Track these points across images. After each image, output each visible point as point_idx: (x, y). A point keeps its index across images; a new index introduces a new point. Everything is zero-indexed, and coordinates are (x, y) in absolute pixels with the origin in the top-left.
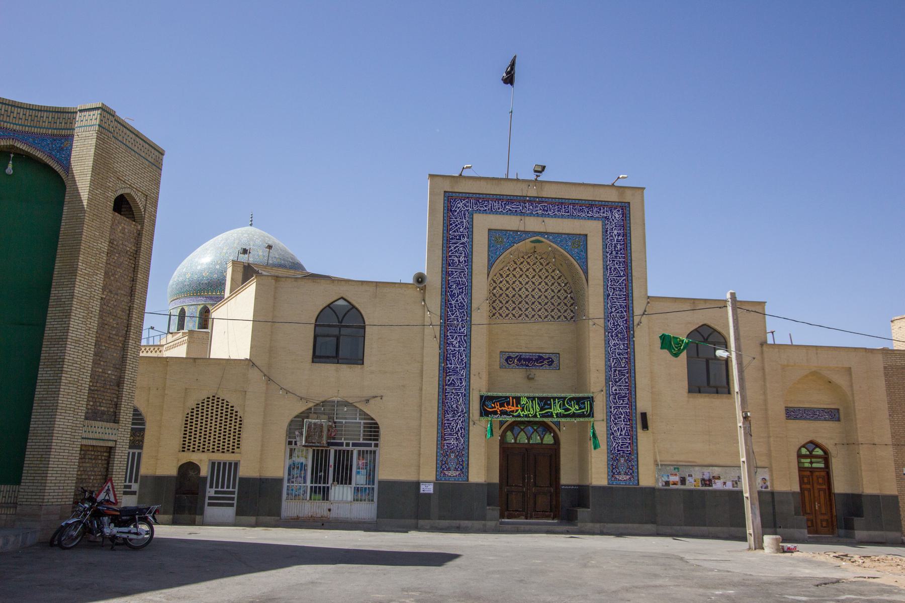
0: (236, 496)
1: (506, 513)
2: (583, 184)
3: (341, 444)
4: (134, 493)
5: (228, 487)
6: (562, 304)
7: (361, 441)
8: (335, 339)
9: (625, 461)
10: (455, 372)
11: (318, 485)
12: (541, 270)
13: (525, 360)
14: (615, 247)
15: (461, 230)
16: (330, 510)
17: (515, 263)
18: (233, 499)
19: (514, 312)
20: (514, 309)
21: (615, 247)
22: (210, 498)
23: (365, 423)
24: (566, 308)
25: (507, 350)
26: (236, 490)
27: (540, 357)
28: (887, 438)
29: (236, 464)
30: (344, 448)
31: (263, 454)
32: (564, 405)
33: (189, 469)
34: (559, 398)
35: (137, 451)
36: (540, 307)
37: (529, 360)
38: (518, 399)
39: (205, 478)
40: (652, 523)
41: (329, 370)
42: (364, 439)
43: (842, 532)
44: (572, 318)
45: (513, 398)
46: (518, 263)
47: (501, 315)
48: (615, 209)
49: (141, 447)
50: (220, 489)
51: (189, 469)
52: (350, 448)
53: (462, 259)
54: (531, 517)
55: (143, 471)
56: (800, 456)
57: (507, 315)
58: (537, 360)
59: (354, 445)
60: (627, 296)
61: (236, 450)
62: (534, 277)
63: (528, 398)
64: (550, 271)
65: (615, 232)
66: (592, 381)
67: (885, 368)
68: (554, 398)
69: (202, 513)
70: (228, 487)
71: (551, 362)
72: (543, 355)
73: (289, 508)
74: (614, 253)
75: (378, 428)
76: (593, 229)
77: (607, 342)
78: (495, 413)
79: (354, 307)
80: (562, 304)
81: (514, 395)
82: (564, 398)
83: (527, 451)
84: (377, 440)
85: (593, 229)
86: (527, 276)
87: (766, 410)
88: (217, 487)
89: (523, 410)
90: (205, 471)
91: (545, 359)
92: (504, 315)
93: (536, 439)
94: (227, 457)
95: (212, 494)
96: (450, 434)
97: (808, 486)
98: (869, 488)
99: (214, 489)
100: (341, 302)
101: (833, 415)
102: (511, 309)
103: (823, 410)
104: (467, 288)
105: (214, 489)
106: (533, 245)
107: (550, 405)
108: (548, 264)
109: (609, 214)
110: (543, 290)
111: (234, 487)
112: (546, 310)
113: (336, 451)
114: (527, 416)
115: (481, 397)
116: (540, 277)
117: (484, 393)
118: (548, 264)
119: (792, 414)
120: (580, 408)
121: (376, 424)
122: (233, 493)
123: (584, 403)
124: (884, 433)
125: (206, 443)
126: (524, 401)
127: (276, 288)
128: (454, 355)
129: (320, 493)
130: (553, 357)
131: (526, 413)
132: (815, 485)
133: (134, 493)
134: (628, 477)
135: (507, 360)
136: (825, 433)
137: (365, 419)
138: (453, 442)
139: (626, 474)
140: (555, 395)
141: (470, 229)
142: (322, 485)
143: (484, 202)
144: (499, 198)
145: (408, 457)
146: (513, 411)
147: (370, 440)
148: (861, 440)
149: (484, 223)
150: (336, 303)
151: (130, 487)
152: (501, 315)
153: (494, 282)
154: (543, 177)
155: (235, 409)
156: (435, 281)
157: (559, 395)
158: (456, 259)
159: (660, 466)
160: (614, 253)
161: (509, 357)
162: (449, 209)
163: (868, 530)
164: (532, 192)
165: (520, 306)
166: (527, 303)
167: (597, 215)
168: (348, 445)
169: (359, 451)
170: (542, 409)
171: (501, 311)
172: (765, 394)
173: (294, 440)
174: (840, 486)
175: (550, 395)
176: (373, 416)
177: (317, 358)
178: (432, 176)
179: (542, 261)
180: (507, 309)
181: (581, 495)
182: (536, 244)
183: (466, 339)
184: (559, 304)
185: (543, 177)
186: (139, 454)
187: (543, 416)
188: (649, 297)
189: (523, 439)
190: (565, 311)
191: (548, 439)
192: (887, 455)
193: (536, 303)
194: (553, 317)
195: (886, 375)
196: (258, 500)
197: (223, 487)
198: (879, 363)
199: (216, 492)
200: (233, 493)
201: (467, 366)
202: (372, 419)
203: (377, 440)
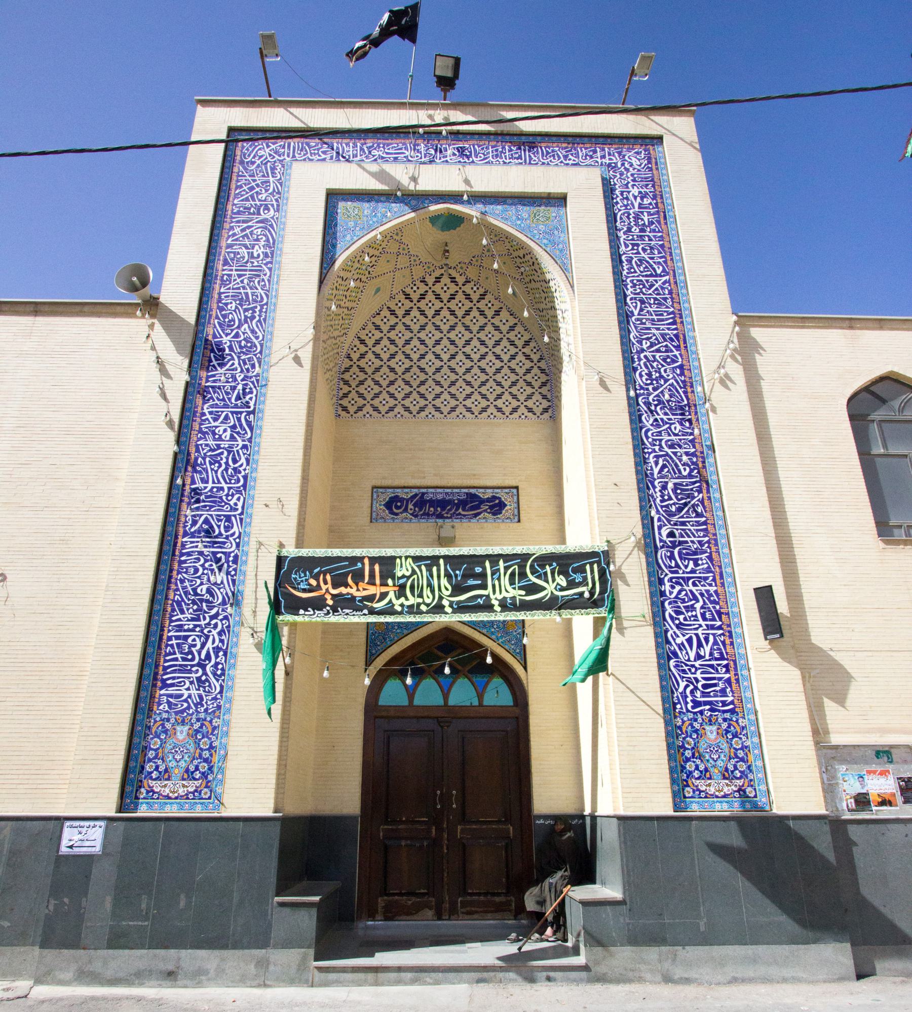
1: (381, 902)
13: (432, 503)
14: (637, 217)
15: (263, 196)
21: (637, 217)
25: (388, 483)
27: (473, 497)
32: (523, 575)
34: (507, 558)
38: (388, 564)
44: (546, 410)
45: (373, 560)
46: (415, 297)
54: (453, 913)
58: (463, 504)
62: (452, 328)
63: (416, 559)
64: (490, 313)
65: (635, 191)
68: (494, 559)
72: (401, 493)
74: (636, 230)
78: (318, 604)
81: (375, 552)
82: (525, 557)
89: (401, 593)
91: (482, 501)
96: (183, 669)
107: (483, 575)
109: (616, 159)
114: (413, 610)
115: (280, 560)
116: (467, 328)
117: (291, 551)
120: (571, 584)
123: (581, 570)
126: (403, 569)
128: (215, 461)
130: (503, 495)
131: (412, 600)
134: (192, 786)
135: (388, 505)
140: (497, 550)
146: (371, 598)
153: (362, 342)
157: (508, 550)
159: (831, 756)
160: (636, 230)
170: (458, 589)
175: (480, 551)
179: (467, 289)
183: (246, 416)
187: (461, 608)
189: (429, 694)
191: (497, 695)
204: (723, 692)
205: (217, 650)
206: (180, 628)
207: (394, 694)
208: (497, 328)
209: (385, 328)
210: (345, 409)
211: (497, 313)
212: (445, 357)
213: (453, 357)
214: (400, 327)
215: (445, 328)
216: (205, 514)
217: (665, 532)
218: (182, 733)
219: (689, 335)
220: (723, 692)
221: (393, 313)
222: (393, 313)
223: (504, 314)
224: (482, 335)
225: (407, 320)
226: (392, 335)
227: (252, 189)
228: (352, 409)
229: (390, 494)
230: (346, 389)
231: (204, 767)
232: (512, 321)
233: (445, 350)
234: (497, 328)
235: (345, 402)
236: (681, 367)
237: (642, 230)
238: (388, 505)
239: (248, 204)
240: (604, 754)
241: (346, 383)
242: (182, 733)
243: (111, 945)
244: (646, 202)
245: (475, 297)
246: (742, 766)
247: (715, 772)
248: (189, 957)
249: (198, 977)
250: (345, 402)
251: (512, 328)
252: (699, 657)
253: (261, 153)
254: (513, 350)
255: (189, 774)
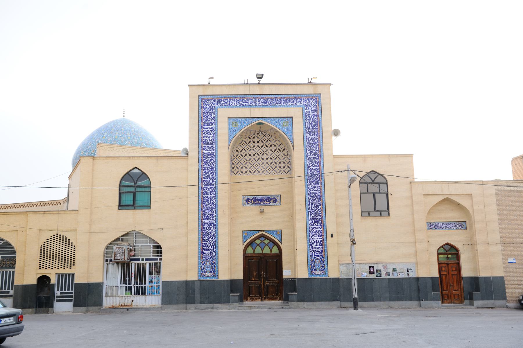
0: (73, 295)
2: (290, 84)
3: (139, 260)
4: (11, 296)
5: (68, 290)
7: (151, 257)
8: (132, 194)
10: (209, 211)
11: (141, 285)
13: (258, 200)
15: (210, 119)
16: (133, 301)
17: (250, 138)
18: (71, 297)
22: (58, 297)
24: (284, 165)
26: (73, 291)
28: (498, 240)
29: (73, 275)
30: (141, 262)
31: (88, 268)
33: (44, 280)
35: (12, 270)
37: (261, 200)
39: (54, 285)
41: (129, 213)
42: (153, 256)
43: (467, 302)
44: (289, 171)
48: (311, 98)
49: (14, 268)
50: (63, 291)
51: (44, 280)
52: (145, 262)
53: (211, 138)
55: (15, 283)
56: (438, 254)
58: (266, 200)
59: (147, 260)
61: (72, 267)
62: (262, 146)
65: (312, 114)
66: (297, 212)
67: (496, 193)
69: (52, 306)
70: (68, 290)
71: (275, 201)
72: (250, 197)
73: (107, 302)
76: (296, 112)
77: (306, 187)
79: (144, 173)
83: (262, 257)
85: (296, 112)
87: (414, 225)
88: (62, 290)
90: (54, 280)
91: (271, 199)
93: (267, 250)
94: (67, 271)
95: (59, 294)
97: (445, 273)
98: (483, 273)
99: (60, 291)
100: (136, 171)
101: (461, 225)
103: (455, 222)
104: (213, 157)
105: (60, 291)
106: (259, 126)
111: (72, 289)
113: (150, 263)
116: (267, 146)
118: (271, 137)
119: (431, 225)
122: (72, 293)
124: (495, 235)
125: (54, 263)
127: (93, 164)
129: (129, 290)
130: (276, 197)
132: (450, 272)
133: (11, 296)
134: (212, 274)
135: (246, 201)
136: (456, 238)
137: (154, 243)
138: (209, 255)
142: (138, 285)
143: (224, 100)
144: (234, 97)
145: (180, 265)
147: (158, 256)
148: (478, 242)
149: (224, 114)
150: (132, 171)
151: (8, 292)
153: (237, 151)
154: (263, 81)
155: (71, 241)
156: (194, 155)
158: (207, 139)
161: (248, 199)
163: (483, 299)
164: (256, 91)
167: (300, 104)
168: (143, 260)
169: (150, 263)
172: (413, 214)
173: (109, 259)
174: (466, 272)
177: (121, 206)
178: (189, 85)
179: (267, 136)
181: (293, 283)
182: (261, 125)
185: (263, 81)
186: (13, 272)
189: (258, 251)
191: (275, 250)
192: (497, 251)
195: (497, 198)
196: (87, 296)
197: (65, 290)
198: (492, 190)
199: (61, 293)
200: (72, 293)
201: (216, 206)
202: (157, 243)
204: (321, 253)
205: (213, 246)
206: (205, 241)
207: (250, 251)
208: (275, 146)
209: (243, 147)
210: (233, 172)
211: (275, 142)
212: (261, 155)
213: (263, 155)
214: (248, 146)
215: (260, 146)
216: (207, 214)
217: (311, 216)
218: (208, 263)
219: (322, 161)
220: (321, 253)
221: (245, 142)
222: (245, 142)
223: (277, 142)
224: (271, 148)
225: (250, 144)
226: (245, 149)
227: (207, 117)
228: (235, 172)
229: (247, 197)
230: (233, 166)
231: (214, 270)
232: (279, 144)
233: (261, 153)
234: (275, 146)
235: (233, 170)
236: (319, 171)
237: (313, 128)
238: (246, 201)
239: (207, 122)
240: (296, 266)
241: (233, 164)
242: (208, 263)
243: (200, 303)
244: (315, 118)
245: (269, 138)
246: (323, 268)
247: (208, 271)
248: (216, 305)
249: (217, 308)
250: (233, 170)
251: (279, 146)
252: (316, 245)
253: (208, 104)
254: (280, 152)
255: (320, 270)
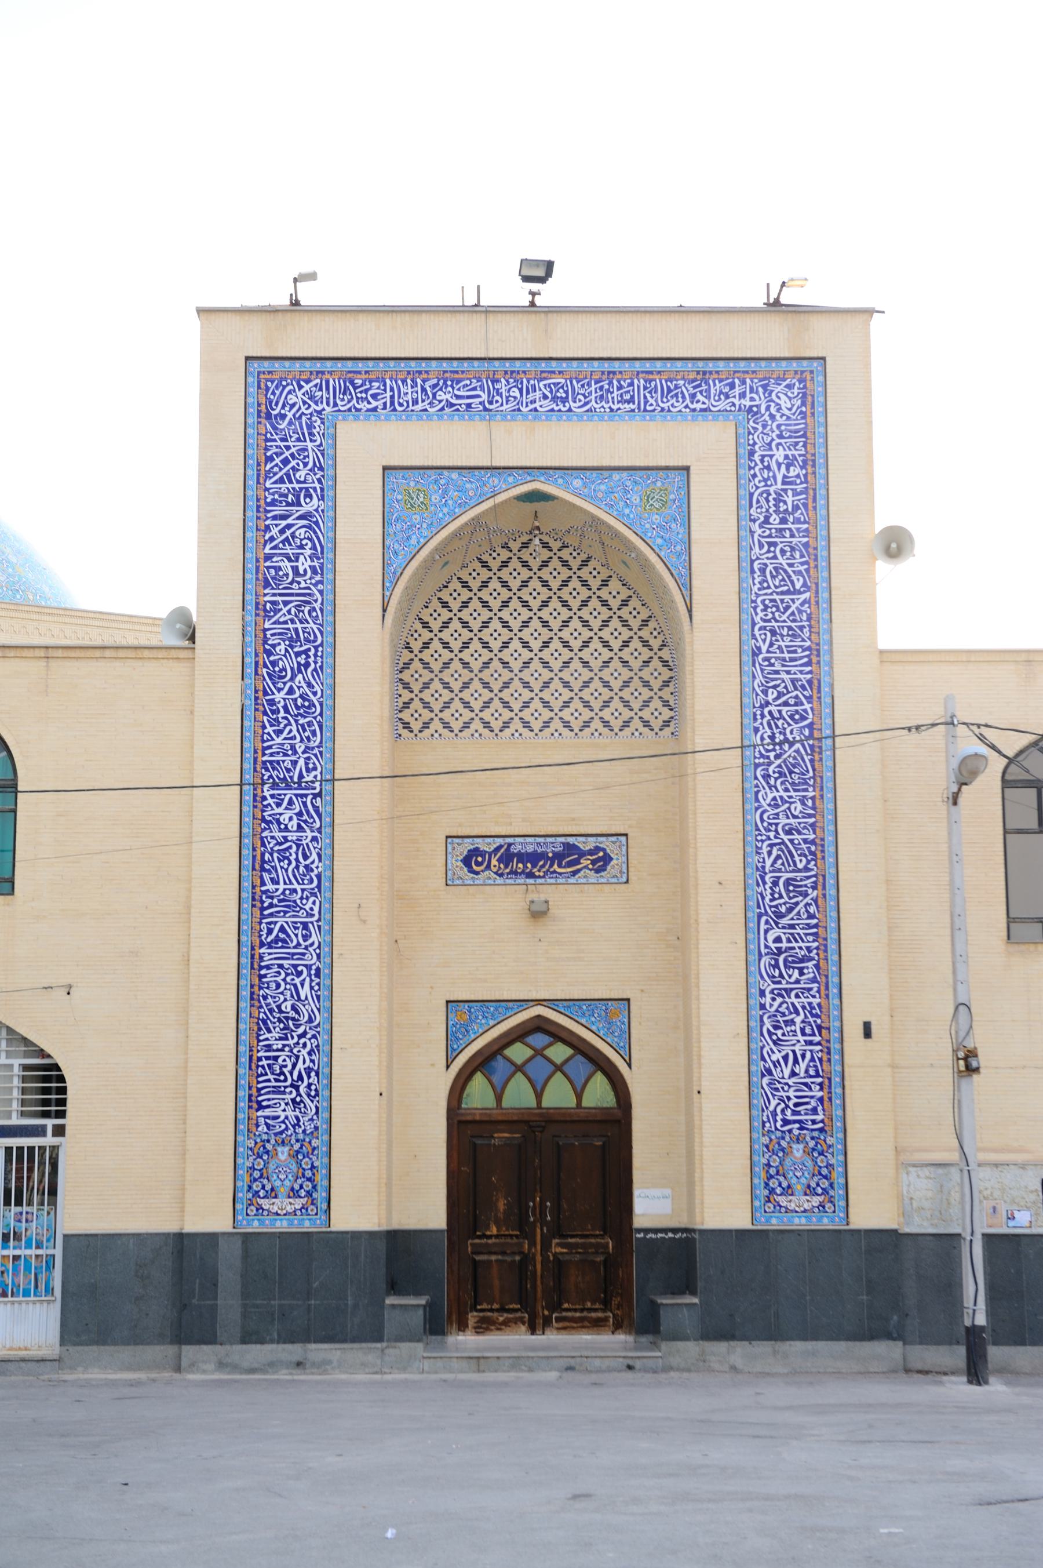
6: (636, 683)
7: (15, 1121)
9: (809, 1152)
10: (289, 905)
12: (565, 583)
13: (522, 857)
15: (301, 474)
17: (485, 565)
19: (486, 715)
20: (487, 705)
21: (778, 500)
23: (26, 1068)
24: (646, 693)
36: (567, 695)
37: (534, 858)
40: (889, 1336)
42: (23, 1114)
44: (666, 723)
46: (495, 565)
47: (447, 726)
48: (779, 380)
53: (303, 564)
57: (546, 724)
58: (558, 857)
60: (814, 653)
64: (595, 584)
65: (780, 455)
71: (602, 862)
72: (579, 842)
74: (775, 519)
75: (61, 1079)
77: (749, 797)
80: (636, 683)
83: (537, 1127)
84: (61, 1114)
86: (525, 604)
91: (582, 854)
92: (536, 725)
93: (559, 1095)
96: (277, 1091)
102: (477, 705)
108: (585, 563)
110: (576, 644)
112: (587, 704)
118: (585, 563)
121: (56, 1067)
130: (605, 843)
134: (816, 1201)
135: (466, 862)
137: (26, 1054)
138: (283, 1111)
139: (809, 1191)
141: (324, 468)
143: (363, 382)
147: (46, 1115)
149: (365, 448)
152: (447, 726)
154: (550, 294)
160: (775, 519)
161: (475, 852)
162: (264, 413)
164: (515, 341)
165: (506, 695)
166: (526, 685)
167: (723, 404)
171: (446, 715)
176: (48, 1049)
178: (200, 311)
179: (565, 554)
180: (467, 705)
181: (683, 1254)
184: (626, 684)
185: (550, 294)
188: (882, 652)
190: (646, 704)
191: (598, 1094)
193: (556, 684)
194: (606, 724)
201: (322, 886)
203: (61, 1114)
